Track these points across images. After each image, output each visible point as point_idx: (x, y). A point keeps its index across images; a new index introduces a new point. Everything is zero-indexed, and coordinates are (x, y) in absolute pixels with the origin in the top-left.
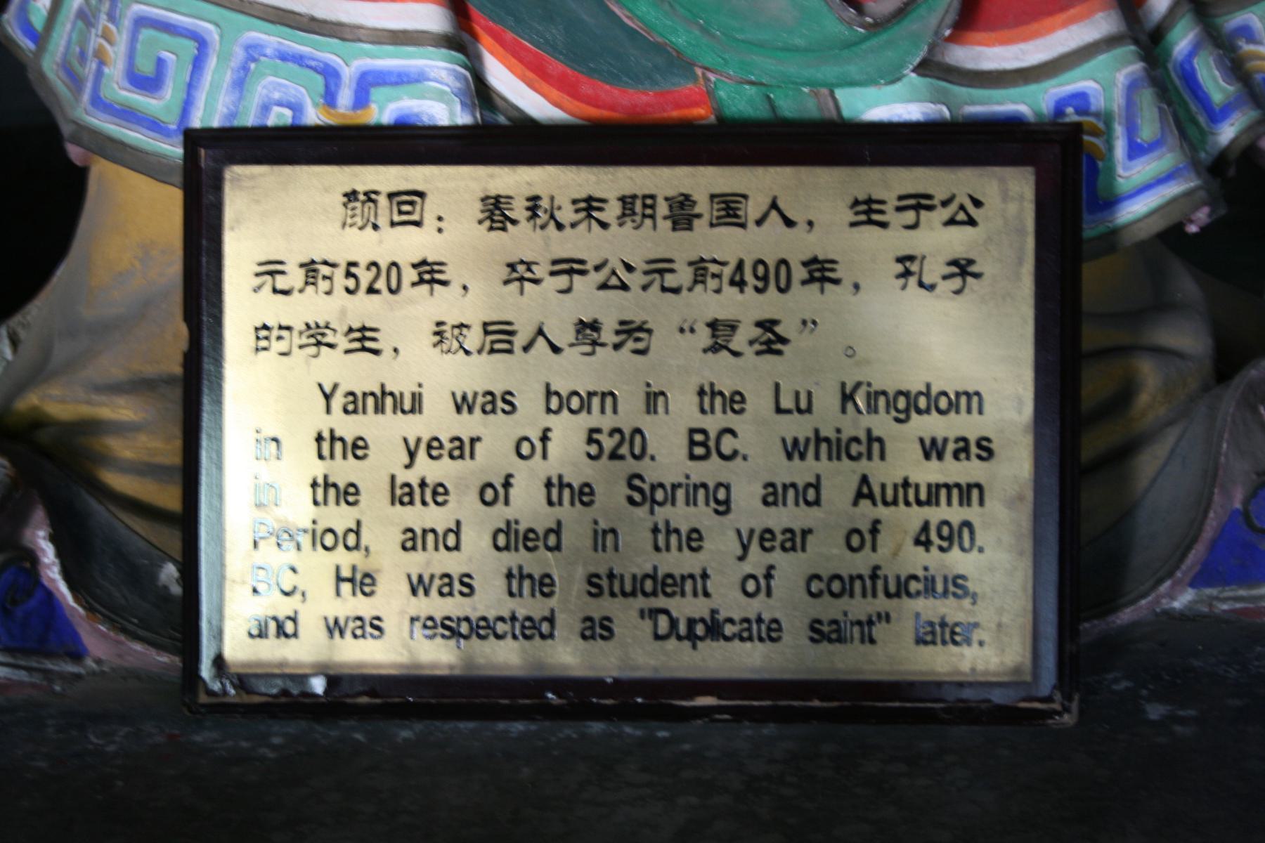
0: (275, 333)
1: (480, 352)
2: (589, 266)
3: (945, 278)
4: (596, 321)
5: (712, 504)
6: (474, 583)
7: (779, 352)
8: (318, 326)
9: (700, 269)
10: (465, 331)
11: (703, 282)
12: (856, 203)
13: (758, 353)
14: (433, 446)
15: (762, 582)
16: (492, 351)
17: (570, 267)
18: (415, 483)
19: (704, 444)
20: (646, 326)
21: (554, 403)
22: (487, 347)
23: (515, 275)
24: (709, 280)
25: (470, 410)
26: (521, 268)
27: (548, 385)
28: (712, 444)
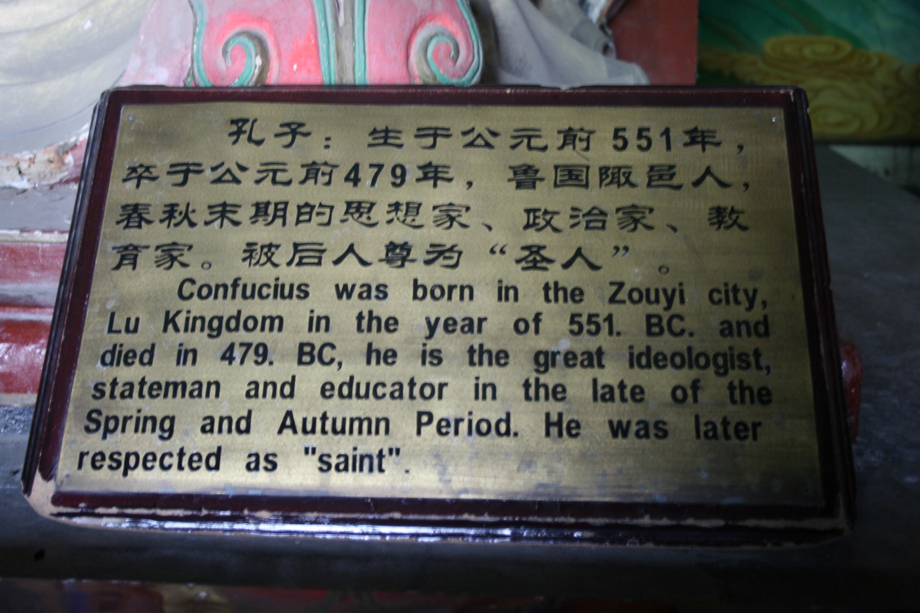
0: (316, 210)
1: (289, 263)
4: (406, 243)
7: (545, 269)
13: (524, 269)
15: (690, 392)
16: (300, 264)
21: (420, 293)
22: (297, 260)
23: (134, 175)
26: (140, 170)
27: (415, 281)
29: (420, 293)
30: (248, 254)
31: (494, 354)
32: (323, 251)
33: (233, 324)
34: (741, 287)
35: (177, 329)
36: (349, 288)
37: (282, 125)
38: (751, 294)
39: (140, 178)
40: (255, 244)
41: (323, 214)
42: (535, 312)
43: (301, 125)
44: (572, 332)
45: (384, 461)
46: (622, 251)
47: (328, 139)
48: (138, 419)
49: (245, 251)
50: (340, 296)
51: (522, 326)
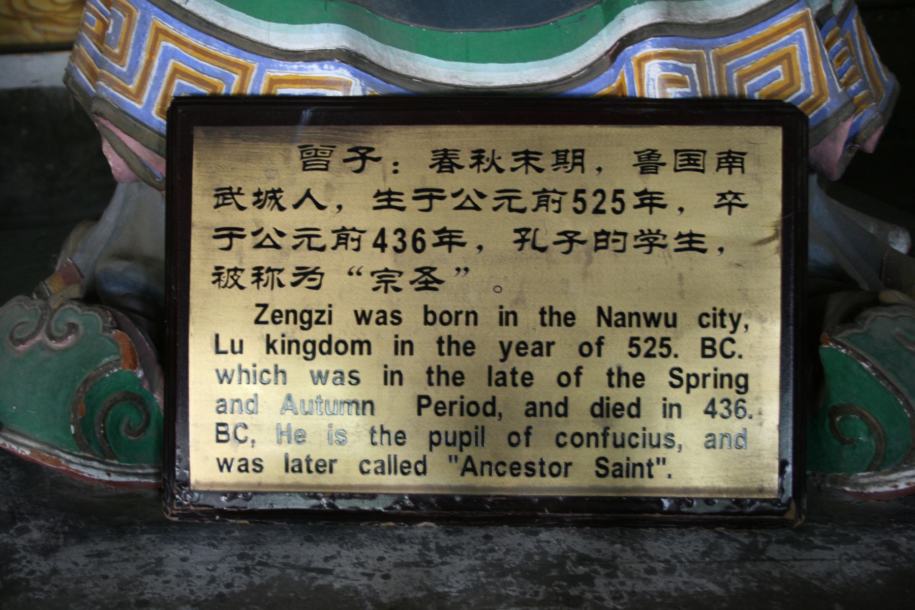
0: (612, 237)
3: (556, 243)
5: (735, 387)
7: (435, 289)
8: (650, 232)
10: (239, 273)
12: (379, 194)
13: (418, 289)
14: (521, 348)
18: (508, 371)
21: (430, 318)
23: (724, 201)
24: (350, 242)
25: (367, 322)
27: (426, 307)
28: (717, 347)
29: (430, 318)
30: (216, 277)
31: (451, 375)
33: (325, 347)
34: (727, 311)
35: (275, 352)
36: (656, 316)
38: (735, 318)
40: (222, 268)
41: (618, 241)
42: (597, 336)
44: (631, 354)
45: (653, 468)
46: (462, 272)
49: (214, 274)
50: (359, 322)
51: (586, 349)
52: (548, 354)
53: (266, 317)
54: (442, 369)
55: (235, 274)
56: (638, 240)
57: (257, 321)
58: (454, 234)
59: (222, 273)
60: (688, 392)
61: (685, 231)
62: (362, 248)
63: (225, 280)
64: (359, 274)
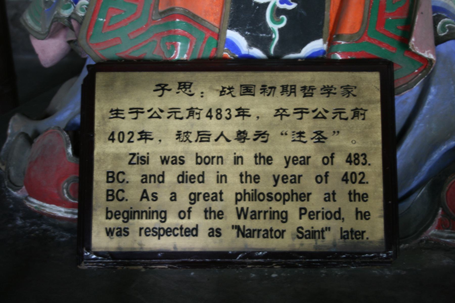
2: (145, 110)
4: (245, 131)
6: (221, 231)
7: (323, 142)
9: (191, 112)
11: (358, 116)
17: (301, 111)
19: (112, 177)
20: (266, 133)
21: (199, 160)
22: (199, 139)
23: (278, 113)
25: (167, 163)
32: (210, 135)
37: (157, 85)
38: (288, 159)
39: (281, 115)
40: (180, 132)
43: (166, 85)
47: (202, 93)
48: (271, 212)
49: (177, 135)
50: (163, 162)
51: (326, 160)
52: (299, 182)
53: (135, 160)
54: (294, 192)
55: (187, 135)
56: (323, 90)
57: (130, 163)
58: (245, 110)
59: (181, 134)
60: (284, 204)
61: (115, 108)
62: (138, 118)
63: (182, 137)
64: (286, 134)
